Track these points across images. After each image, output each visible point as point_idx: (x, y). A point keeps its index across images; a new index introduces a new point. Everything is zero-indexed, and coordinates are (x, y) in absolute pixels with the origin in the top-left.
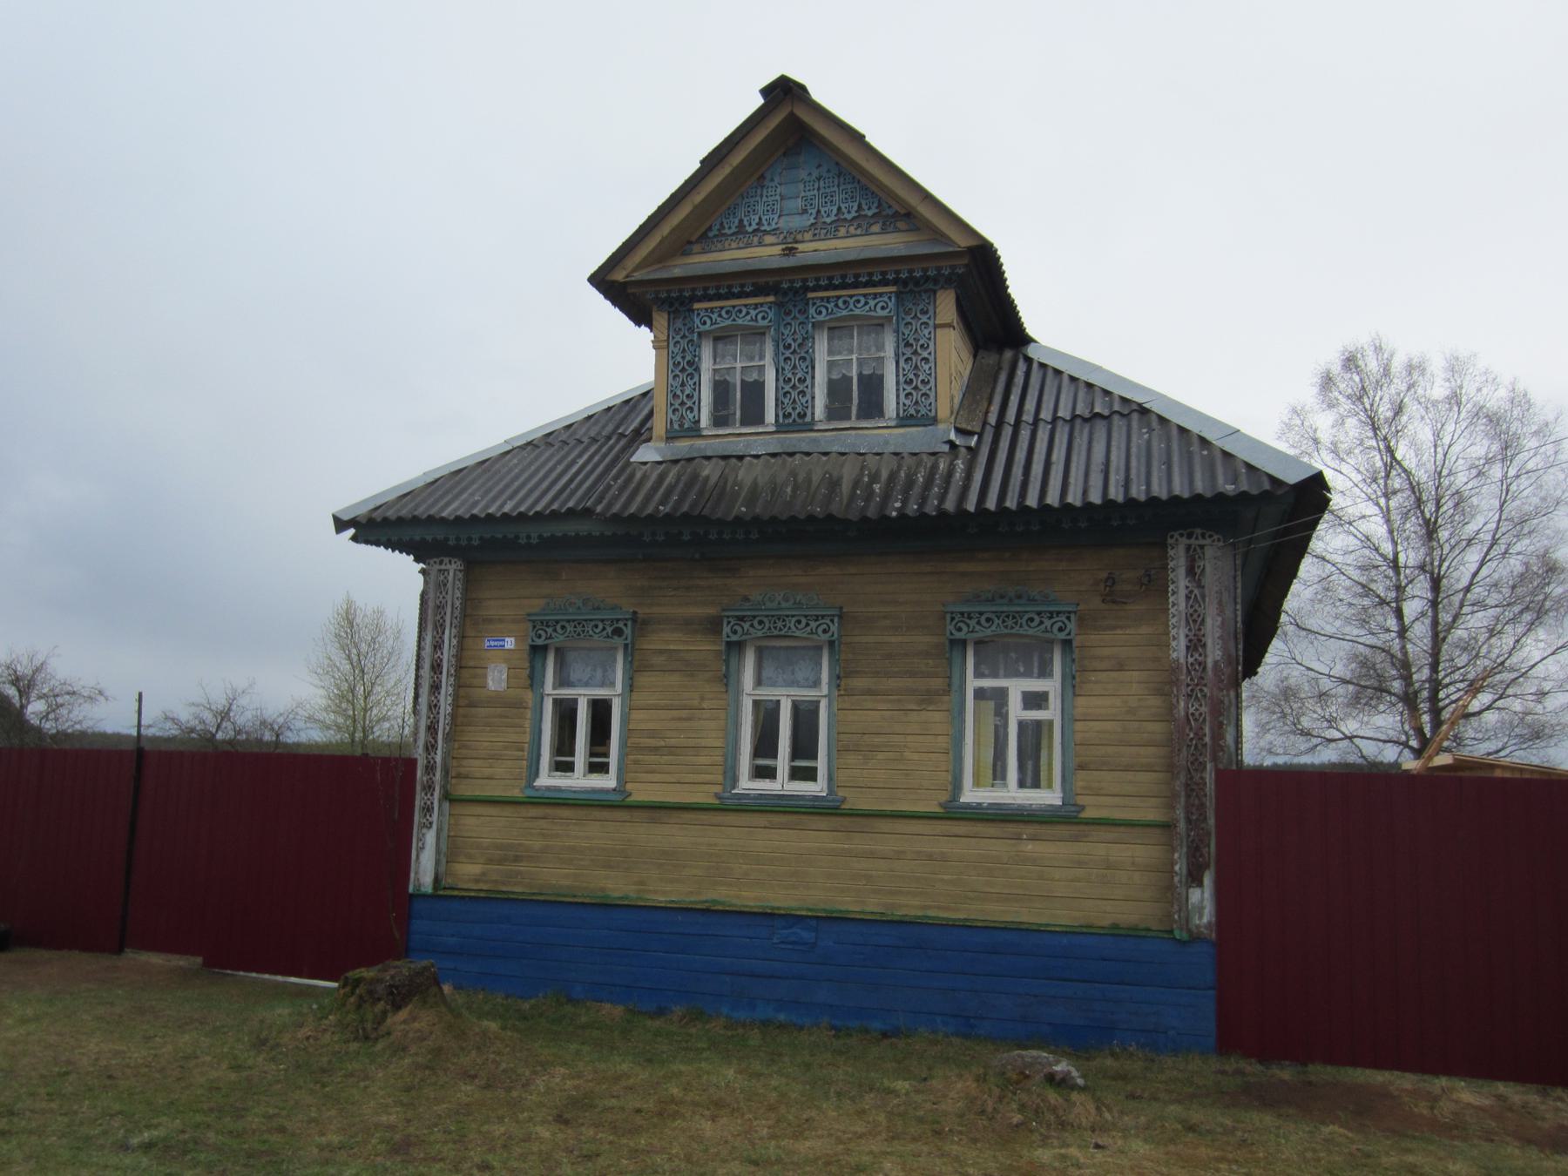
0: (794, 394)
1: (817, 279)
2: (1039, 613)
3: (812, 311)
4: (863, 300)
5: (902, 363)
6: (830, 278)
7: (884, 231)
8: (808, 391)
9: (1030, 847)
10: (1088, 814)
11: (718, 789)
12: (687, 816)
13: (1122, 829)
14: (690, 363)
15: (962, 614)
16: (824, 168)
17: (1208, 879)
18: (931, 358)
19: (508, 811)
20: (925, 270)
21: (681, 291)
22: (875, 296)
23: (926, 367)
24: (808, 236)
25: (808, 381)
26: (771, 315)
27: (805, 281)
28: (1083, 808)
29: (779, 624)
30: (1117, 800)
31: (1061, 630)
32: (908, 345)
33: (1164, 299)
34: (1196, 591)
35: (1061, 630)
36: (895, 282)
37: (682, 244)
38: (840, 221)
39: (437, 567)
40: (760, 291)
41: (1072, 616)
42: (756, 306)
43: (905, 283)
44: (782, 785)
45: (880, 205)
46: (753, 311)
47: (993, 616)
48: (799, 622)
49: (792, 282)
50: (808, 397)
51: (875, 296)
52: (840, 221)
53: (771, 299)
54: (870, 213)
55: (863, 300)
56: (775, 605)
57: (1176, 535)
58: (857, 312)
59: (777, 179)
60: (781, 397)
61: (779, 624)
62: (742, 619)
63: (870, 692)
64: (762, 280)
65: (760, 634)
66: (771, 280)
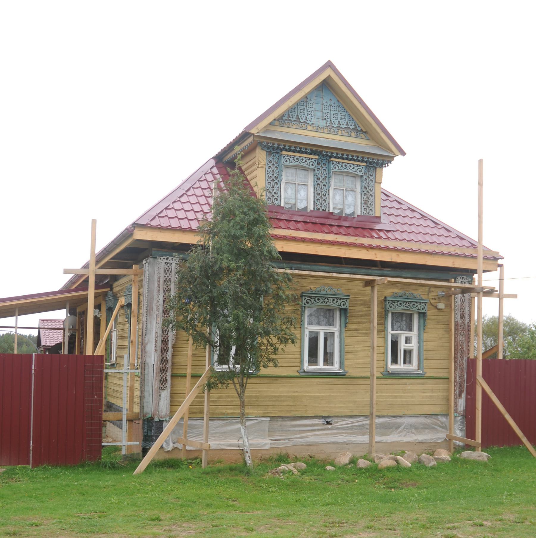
0: (321, 200)
1: (337, 154)
2: (416, 302)
3: (283, 160)
4: (352, 166)
5: (363, 195)
6: (342, 155)
7: (357, 136)
8: (327, 200)
9: (409, 387)
10: (427, 375)
11: (298, 369)
12: (280, 380)
13: (437, 380)
14: (276, 178)
15: (392, 301)
16: (333, 102)
17: (464, 395)
18: (373, 195)
19: (439, 380)
20: (279, 145)
21: (273, 144)
22: (357, 166)
23: (372, 198)
24: (326, 131)
25: (327, 196)
26: (363, 170)
27: (332, 153)
28: (426, 373)
29: (326, 300)
30: (435, 370)
31: (423, 309)
32: (365, 188)
33: (426, 185)
34: (463, 298)
35: (344, 305)
36: (366, 162)
37: (281, 120)
38: (339, 128)
39: (165, 261)
40: (313, 153)
41: (348, 300)
42: (309, 159)
43: (370, 163)
44: (321, 366)
45: (355, 125)
46: (309, 160)
47: (401, 302)
48: (334, 300)
49: (327, 152)
50: (327, 203)
51: (357, 166)
52: (339, 128)
53: (317, 157)
54: (351, 127)
55: (352, 166)
56: (406, 297)
57: (459, 277)
58: (350, 171)
59: (313, 101)
60: (316, 201)
61: (407, 305)
62: (310, 297)
63: (356, 330)
64: (314, 149)
65: (318, 304)
66: (319, 149)
